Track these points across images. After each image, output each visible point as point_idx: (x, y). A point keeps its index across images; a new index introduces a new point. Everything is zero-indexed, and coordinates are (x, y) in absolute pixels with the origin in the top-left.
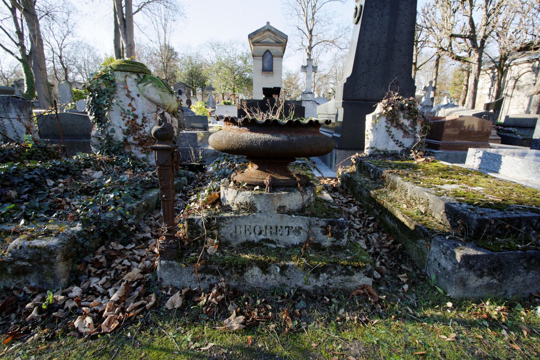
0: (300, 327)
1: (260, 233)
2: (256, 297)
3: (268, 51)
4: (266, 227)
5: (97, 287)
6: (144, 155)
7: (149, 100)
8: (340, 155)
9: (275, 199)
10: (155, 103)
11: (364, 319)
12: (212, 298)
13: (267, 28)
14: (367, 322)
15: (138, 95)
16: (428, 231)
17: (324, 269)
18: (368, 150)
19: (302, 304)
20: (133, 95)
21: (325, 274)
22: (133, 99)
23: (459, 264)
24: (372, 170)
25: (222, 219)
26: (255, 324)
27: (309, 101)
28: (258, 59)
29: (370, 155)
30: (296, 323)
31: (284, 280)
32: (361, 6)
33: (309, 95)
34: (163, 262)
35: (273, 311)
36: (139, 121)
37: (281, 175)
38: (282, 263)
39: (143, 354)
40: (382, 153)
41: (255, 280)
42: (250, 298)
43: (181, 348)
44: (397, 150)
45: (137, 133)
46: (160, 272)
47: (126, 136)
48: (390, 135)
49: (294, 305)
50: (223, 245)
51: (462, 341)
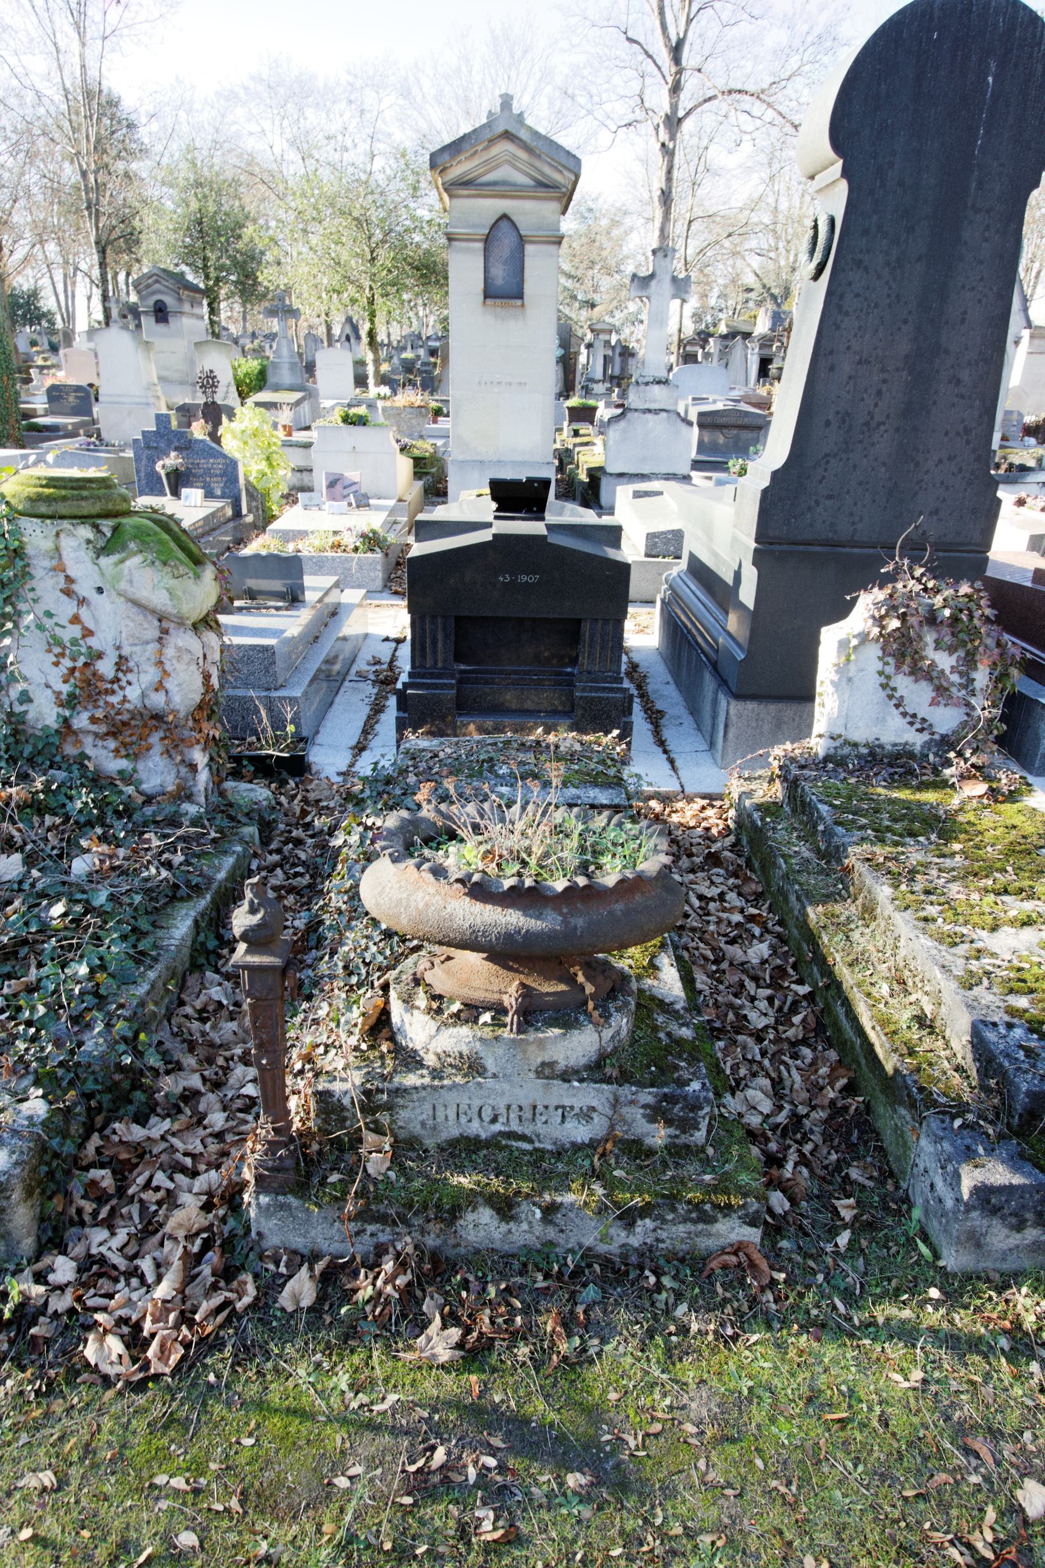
0: (585, 1350)
1: (494, 1120)
2: (485, 1275)
3: (505, 217)
4: (509, 1107)
5: (108, 1254)
6: (123, 764)
7: (136, 603)
8: (740, 716)
9: (532, 1048)
10: (153, 612)
11: (729, 1331)
12: (385, 1283)
13: (501, 129)
14: (735, 1338)
15: (100, 590)
16: (919, 1097)
17: (645, 1211)
18: (822, 741)
19: (591, 1293)
20: (84, 588)
21: (647, 1221)
22: (82, 602)
23: (966, 1204)
24: (821, 828)
25: (400, 1092)
26: (486, 1345)
27: (657, 412)
28: (468, 250)
29: (827, 759)
30: (577, 1341)
31: (551, 1233)
32: (832, 221)
33: (656, 388)
34: (264, 1199)
35: (525, 1312)
36: (106, 667)
37: (548, 978)
38: (547, 1197)
39: (253, 1424)
40: (864, 751)
41: (482, 1233)
42: (471, 1278)
43: (329, 1406)
44: (911, 741)
45: (101, 703)
46: (257, 1221)
47: (67, 713)
48: (890, 697)
49: (573, 1295)
50: (405, 1147)
51: (933, 1388)
